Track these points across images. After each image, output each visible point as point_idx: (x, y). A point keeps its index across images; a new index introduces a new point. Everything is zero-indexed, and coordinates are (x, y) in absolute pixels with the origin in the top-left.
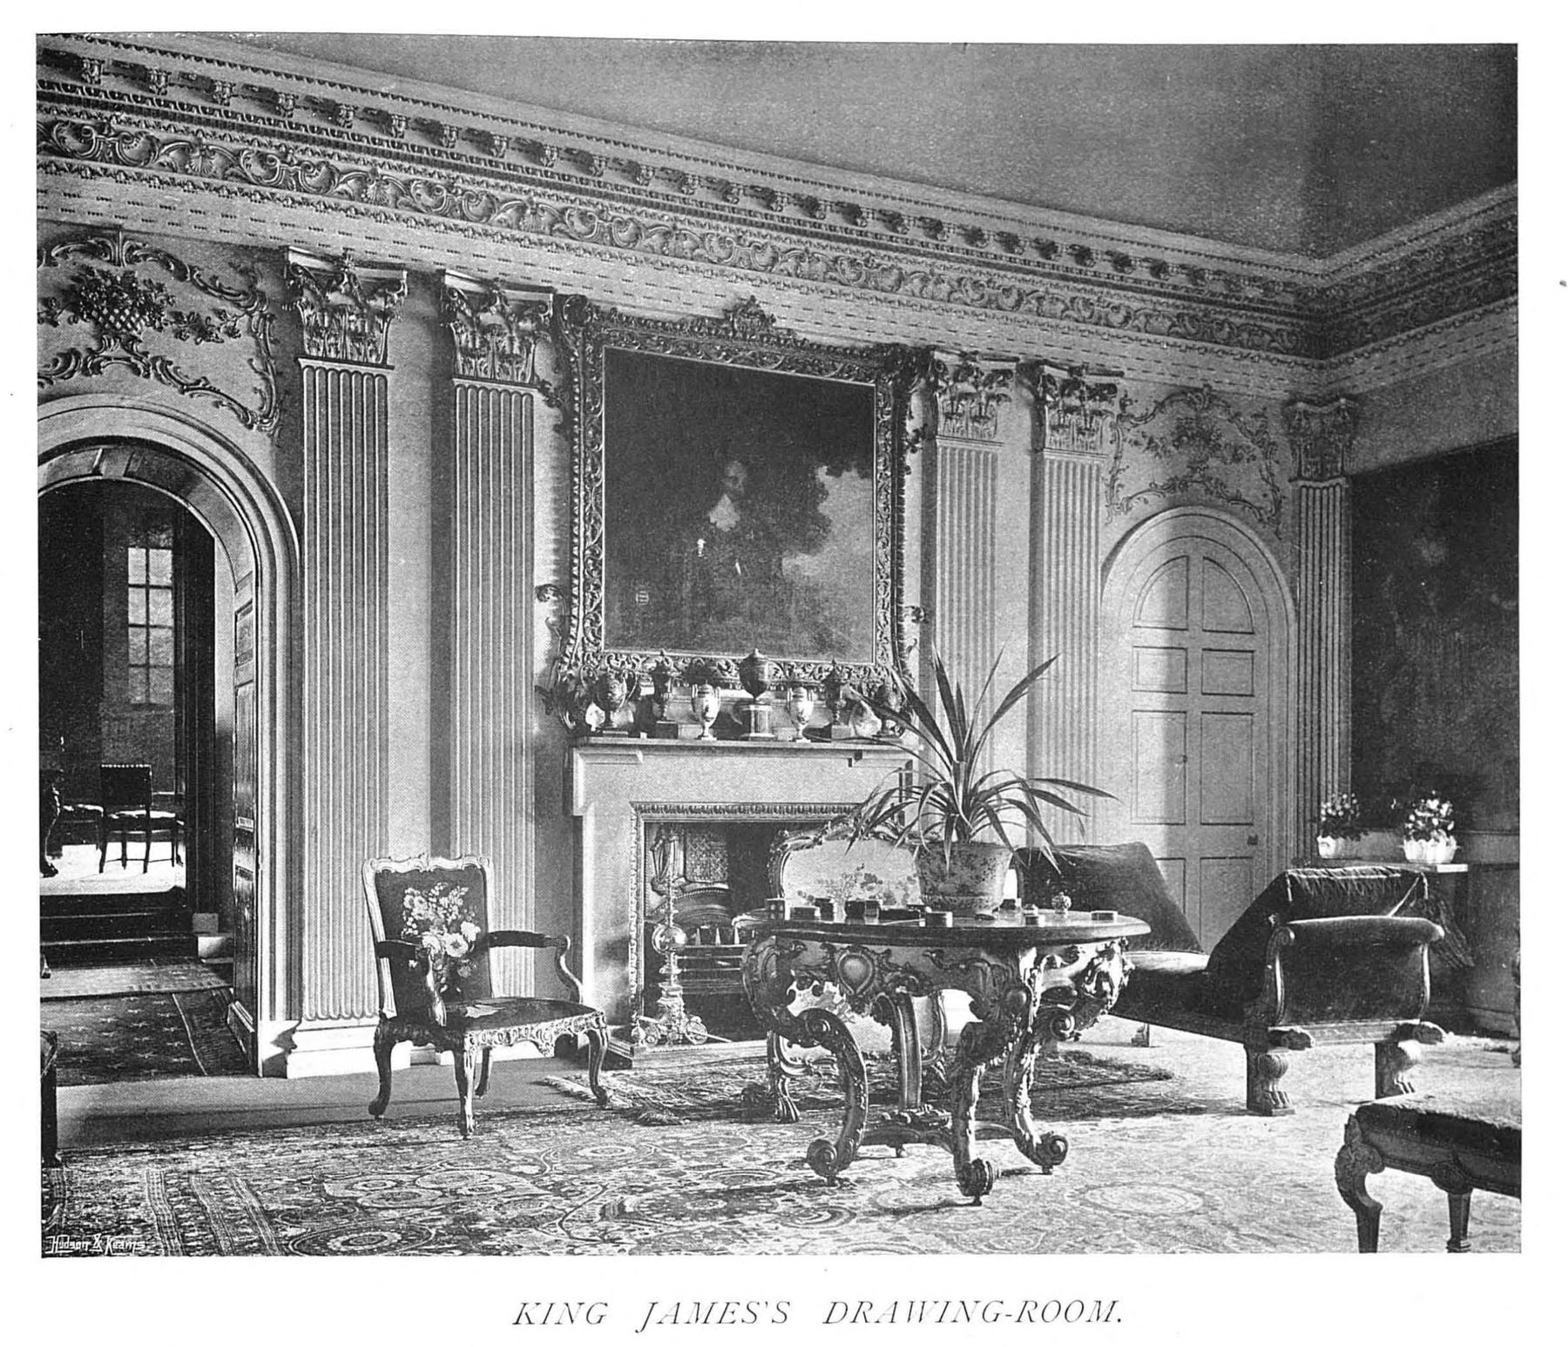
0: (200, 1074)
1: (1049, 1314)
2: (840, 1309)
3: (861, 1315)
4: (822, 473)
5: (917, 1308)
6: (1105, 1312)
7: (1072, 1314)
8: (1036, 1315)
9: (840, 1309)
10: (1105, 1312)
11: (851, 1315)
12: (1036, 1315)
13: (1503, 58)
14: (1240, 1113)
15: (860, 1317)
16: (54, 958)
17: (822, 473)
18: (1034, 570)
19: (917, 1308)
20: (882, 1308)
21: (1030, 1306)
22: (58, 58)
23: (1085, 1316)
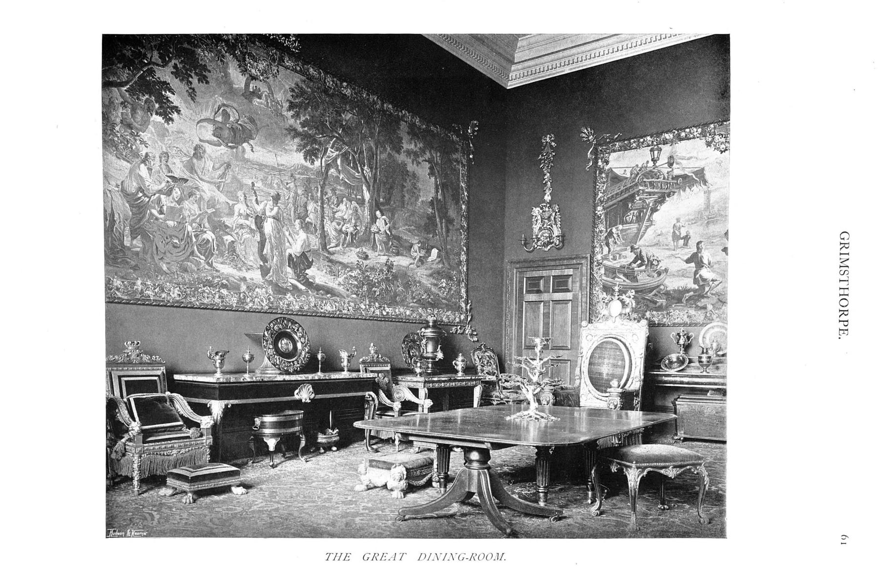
2: (423, 556)
5: (337, 558)
6: (500, 557)
8: (476, 558)
9: (423, 556)
10: (500, 557)
12: (476, 558)
19: (337, 558)
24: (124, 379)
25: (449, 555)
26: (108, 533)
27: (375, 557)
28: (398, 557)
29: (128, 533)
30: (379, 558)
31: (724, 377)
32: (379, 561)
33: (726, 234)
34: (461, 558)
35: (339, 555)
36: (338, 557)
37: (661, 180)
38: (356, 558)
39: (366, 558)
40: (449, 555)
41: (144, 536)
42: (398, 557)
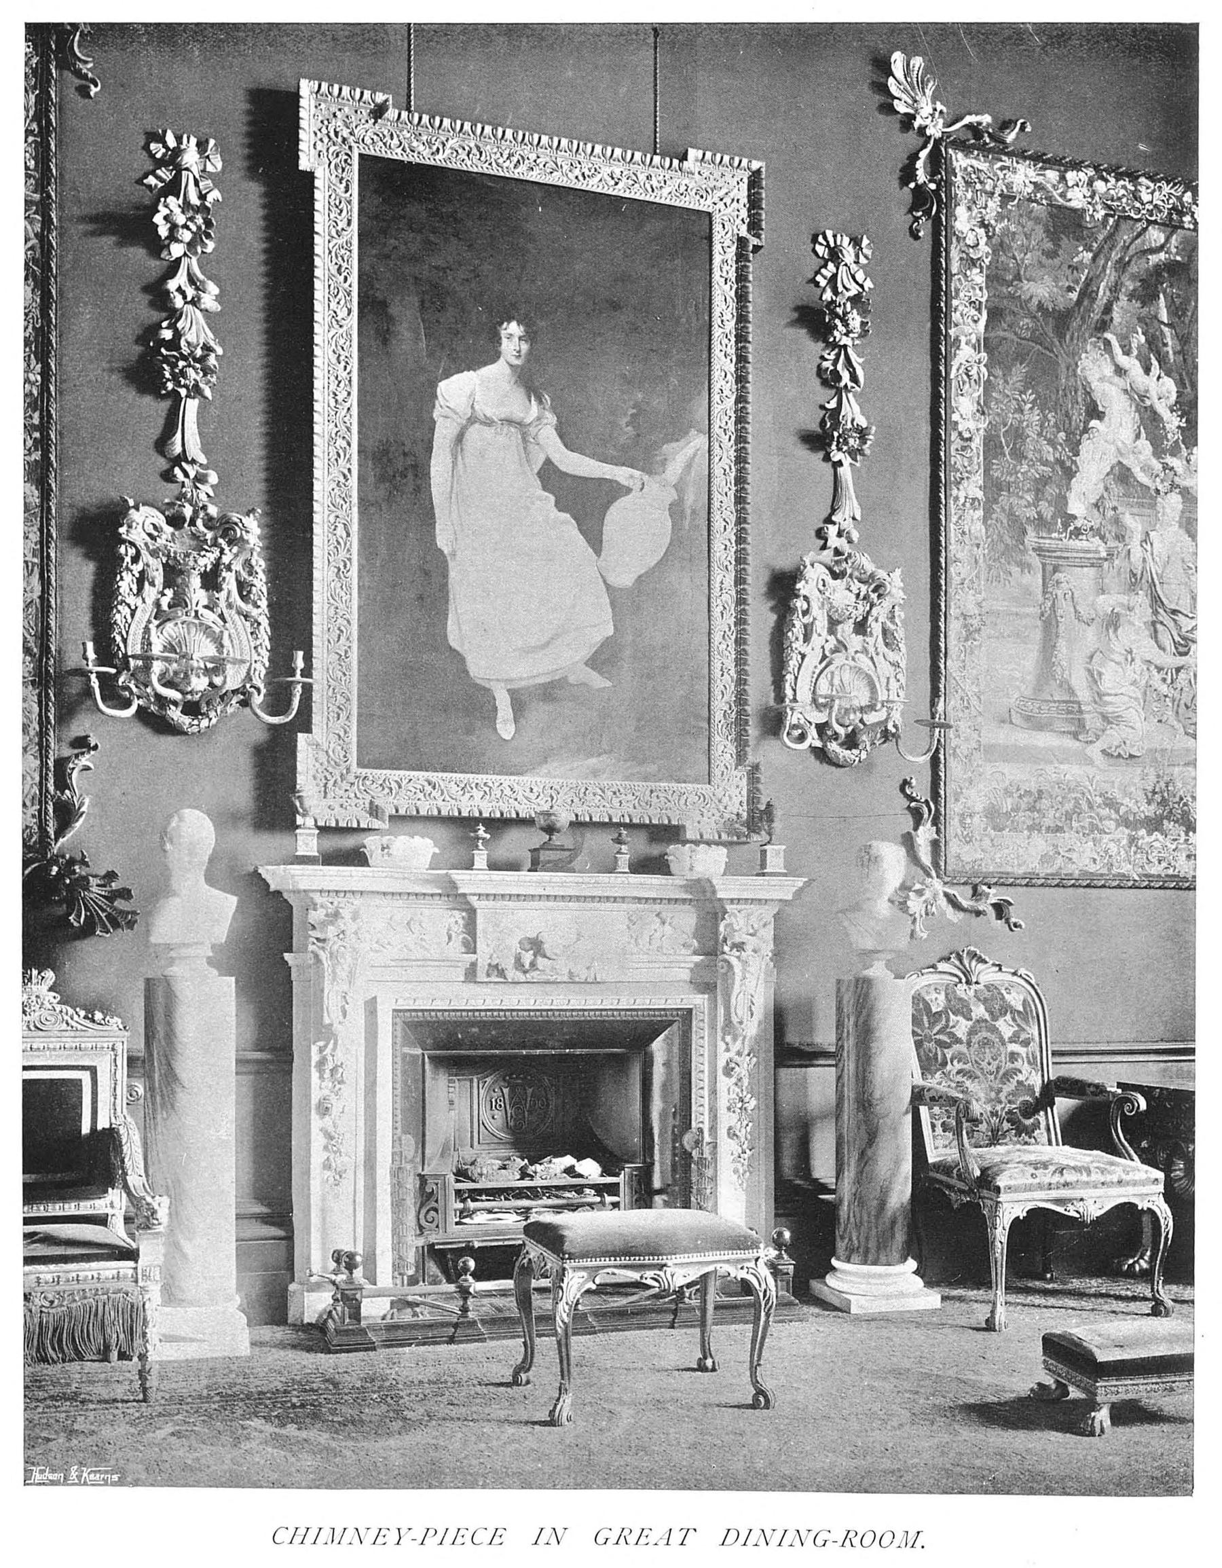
0: (749, 190)
1: (866, 1542)
2: (733, 1534)
3: (848, 1540)
4: (437, 851)
5: (298, 1539)
6: (913, 1540)
7: (885, 1542)
8: (856, 1541)
9: (733, 1534)
10: (913, 1540)
11: (742, 1540)
12: (856, 1541)
13: (1195, 27)
14: (693, 1370)
15: (622, 1540)
16: (25, 1224)
17: (437, 851)
18: (578, 898)
19: (298, 1539)
20: (657, 1534)
21: (852, 1535)
22: (37, 33)
23: (897, 1542)
24: (85, 1077)
25: (351, 1532)
26: (28, 1475)
27: (622, 1538)
28: (677, 1537)
29: (74, 1474)
30: (632, 1539)
31: (28, 1260)
32: (632, 1547)
33: (24, 1012)
34: (819, 1541)
35: (302, 1531)
36: (300, 1536)
37: (272, 770)
38: (578, 1539)
39: (601, 1540)
40: (351, 1532)
41: (114, 1484)
42: (677, 1537)
